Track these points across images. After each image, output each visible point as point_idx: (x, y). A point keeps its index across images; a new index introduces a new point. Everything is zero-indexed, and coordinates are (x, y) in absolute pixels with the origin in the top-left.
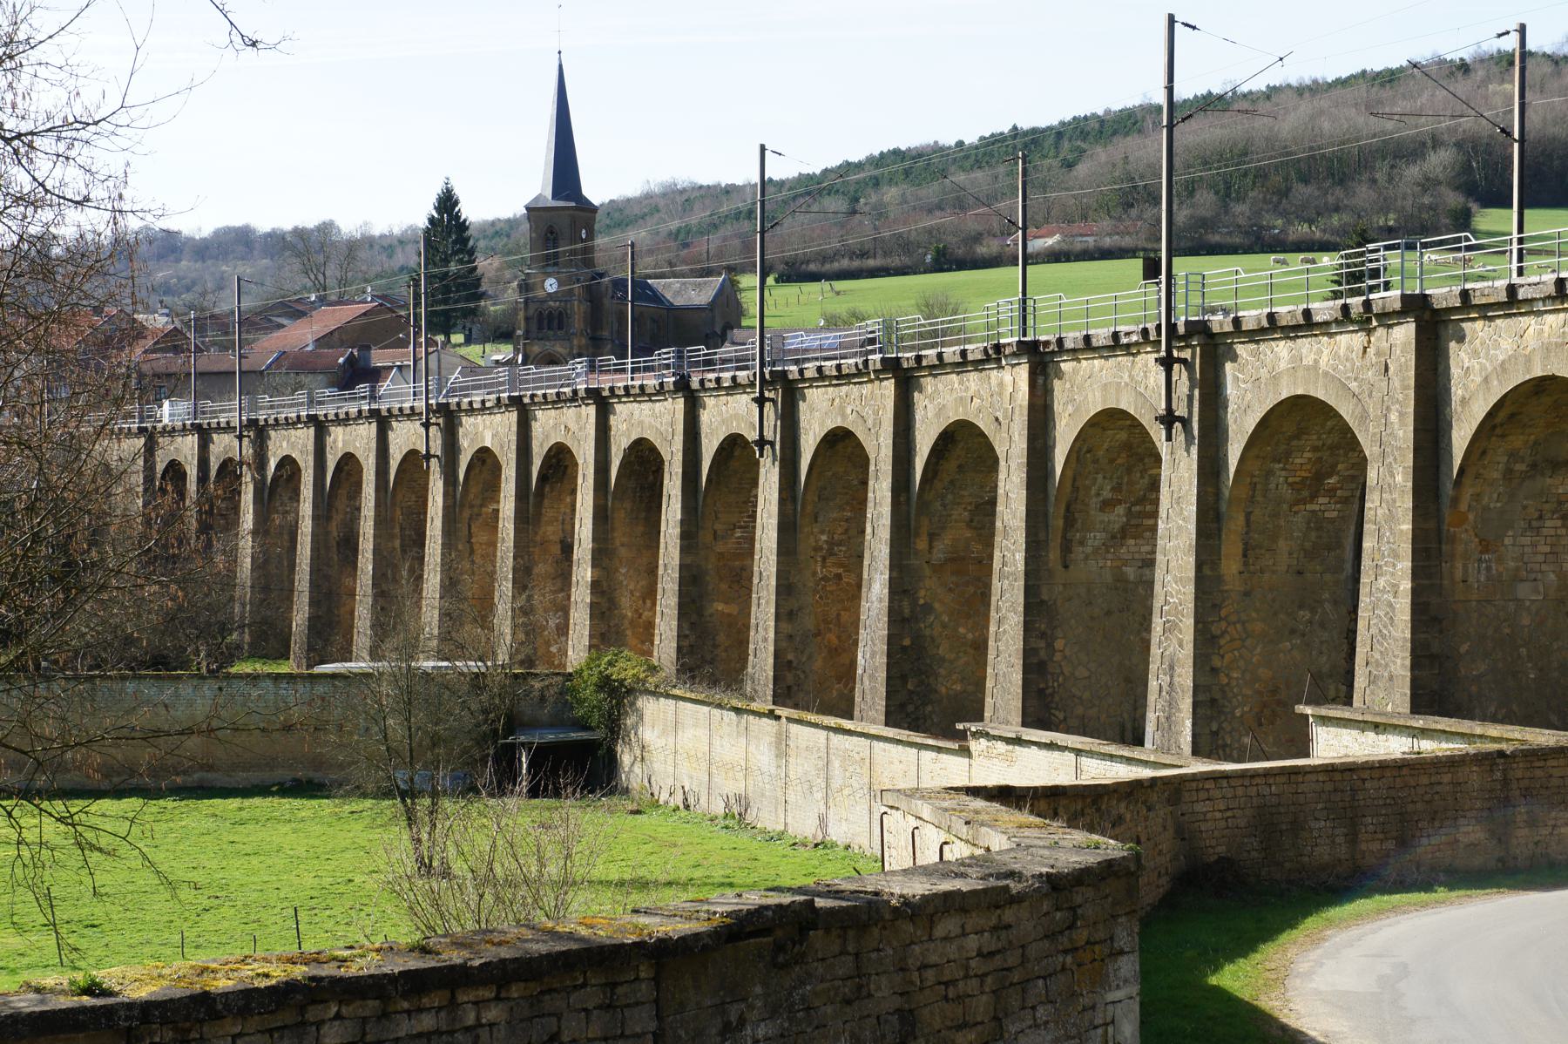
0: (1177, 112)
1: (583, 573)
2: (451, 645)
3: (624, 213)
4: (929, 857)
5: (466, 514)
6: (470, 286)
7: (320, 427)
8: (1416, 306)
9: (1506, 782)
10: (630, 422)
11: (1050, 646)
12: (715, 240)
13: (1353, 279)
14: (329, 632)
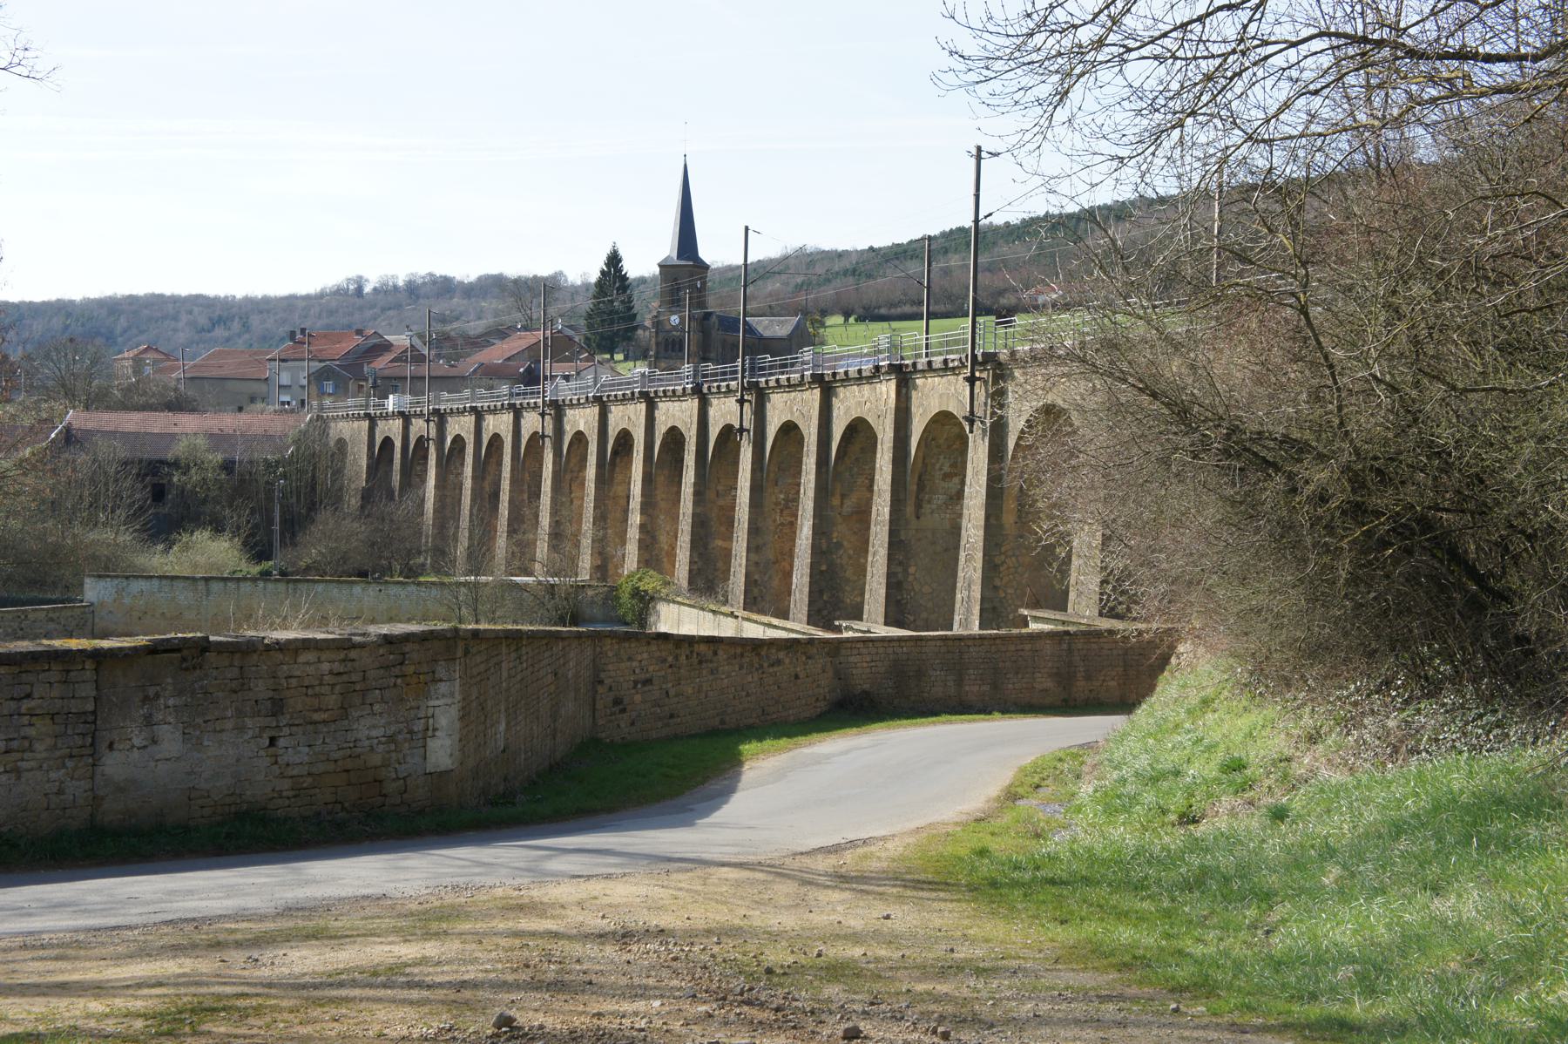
5: (568, 477)
6: (629, 316)
7: (479, 415)
9: (1070, 650)
11: (906, 571)
14: (479, 558)
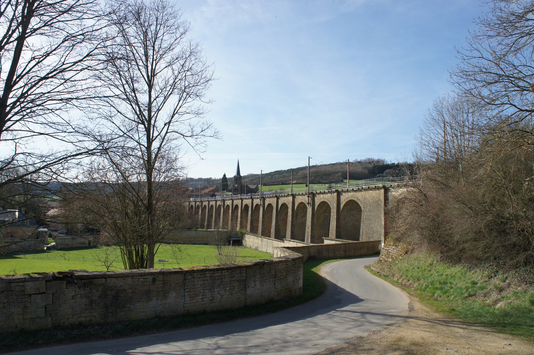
0: (310, 167)
1: (239, 220)
2: (223, 228)
3: (245, 177)
4: (279, 256)
6: (227, 186)
7: (209, 201)
8: (337, 191)
10: (245, 202)
12: (256, 181)
13: (330, 188)
14: (209, 226)
